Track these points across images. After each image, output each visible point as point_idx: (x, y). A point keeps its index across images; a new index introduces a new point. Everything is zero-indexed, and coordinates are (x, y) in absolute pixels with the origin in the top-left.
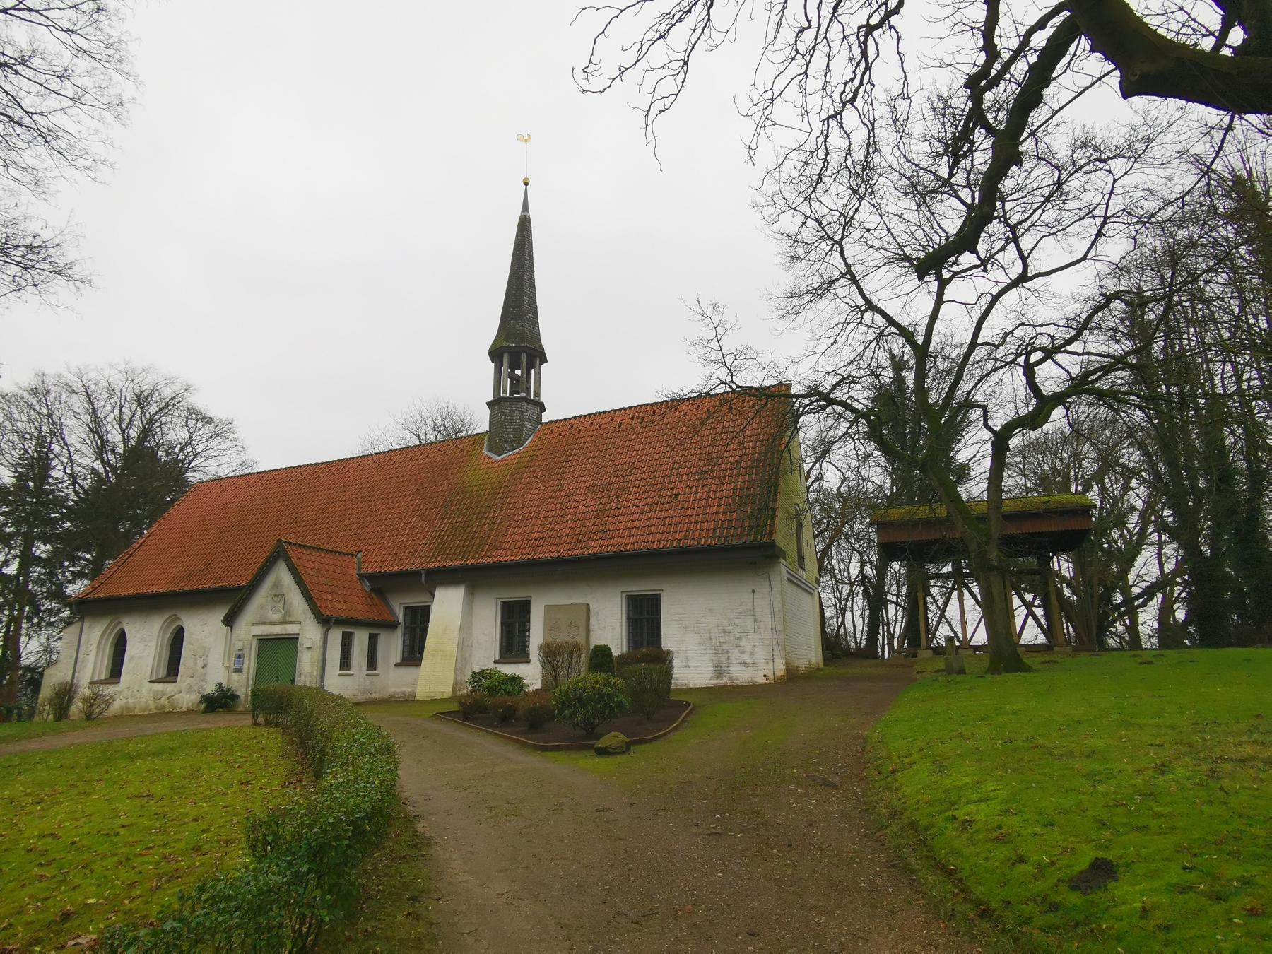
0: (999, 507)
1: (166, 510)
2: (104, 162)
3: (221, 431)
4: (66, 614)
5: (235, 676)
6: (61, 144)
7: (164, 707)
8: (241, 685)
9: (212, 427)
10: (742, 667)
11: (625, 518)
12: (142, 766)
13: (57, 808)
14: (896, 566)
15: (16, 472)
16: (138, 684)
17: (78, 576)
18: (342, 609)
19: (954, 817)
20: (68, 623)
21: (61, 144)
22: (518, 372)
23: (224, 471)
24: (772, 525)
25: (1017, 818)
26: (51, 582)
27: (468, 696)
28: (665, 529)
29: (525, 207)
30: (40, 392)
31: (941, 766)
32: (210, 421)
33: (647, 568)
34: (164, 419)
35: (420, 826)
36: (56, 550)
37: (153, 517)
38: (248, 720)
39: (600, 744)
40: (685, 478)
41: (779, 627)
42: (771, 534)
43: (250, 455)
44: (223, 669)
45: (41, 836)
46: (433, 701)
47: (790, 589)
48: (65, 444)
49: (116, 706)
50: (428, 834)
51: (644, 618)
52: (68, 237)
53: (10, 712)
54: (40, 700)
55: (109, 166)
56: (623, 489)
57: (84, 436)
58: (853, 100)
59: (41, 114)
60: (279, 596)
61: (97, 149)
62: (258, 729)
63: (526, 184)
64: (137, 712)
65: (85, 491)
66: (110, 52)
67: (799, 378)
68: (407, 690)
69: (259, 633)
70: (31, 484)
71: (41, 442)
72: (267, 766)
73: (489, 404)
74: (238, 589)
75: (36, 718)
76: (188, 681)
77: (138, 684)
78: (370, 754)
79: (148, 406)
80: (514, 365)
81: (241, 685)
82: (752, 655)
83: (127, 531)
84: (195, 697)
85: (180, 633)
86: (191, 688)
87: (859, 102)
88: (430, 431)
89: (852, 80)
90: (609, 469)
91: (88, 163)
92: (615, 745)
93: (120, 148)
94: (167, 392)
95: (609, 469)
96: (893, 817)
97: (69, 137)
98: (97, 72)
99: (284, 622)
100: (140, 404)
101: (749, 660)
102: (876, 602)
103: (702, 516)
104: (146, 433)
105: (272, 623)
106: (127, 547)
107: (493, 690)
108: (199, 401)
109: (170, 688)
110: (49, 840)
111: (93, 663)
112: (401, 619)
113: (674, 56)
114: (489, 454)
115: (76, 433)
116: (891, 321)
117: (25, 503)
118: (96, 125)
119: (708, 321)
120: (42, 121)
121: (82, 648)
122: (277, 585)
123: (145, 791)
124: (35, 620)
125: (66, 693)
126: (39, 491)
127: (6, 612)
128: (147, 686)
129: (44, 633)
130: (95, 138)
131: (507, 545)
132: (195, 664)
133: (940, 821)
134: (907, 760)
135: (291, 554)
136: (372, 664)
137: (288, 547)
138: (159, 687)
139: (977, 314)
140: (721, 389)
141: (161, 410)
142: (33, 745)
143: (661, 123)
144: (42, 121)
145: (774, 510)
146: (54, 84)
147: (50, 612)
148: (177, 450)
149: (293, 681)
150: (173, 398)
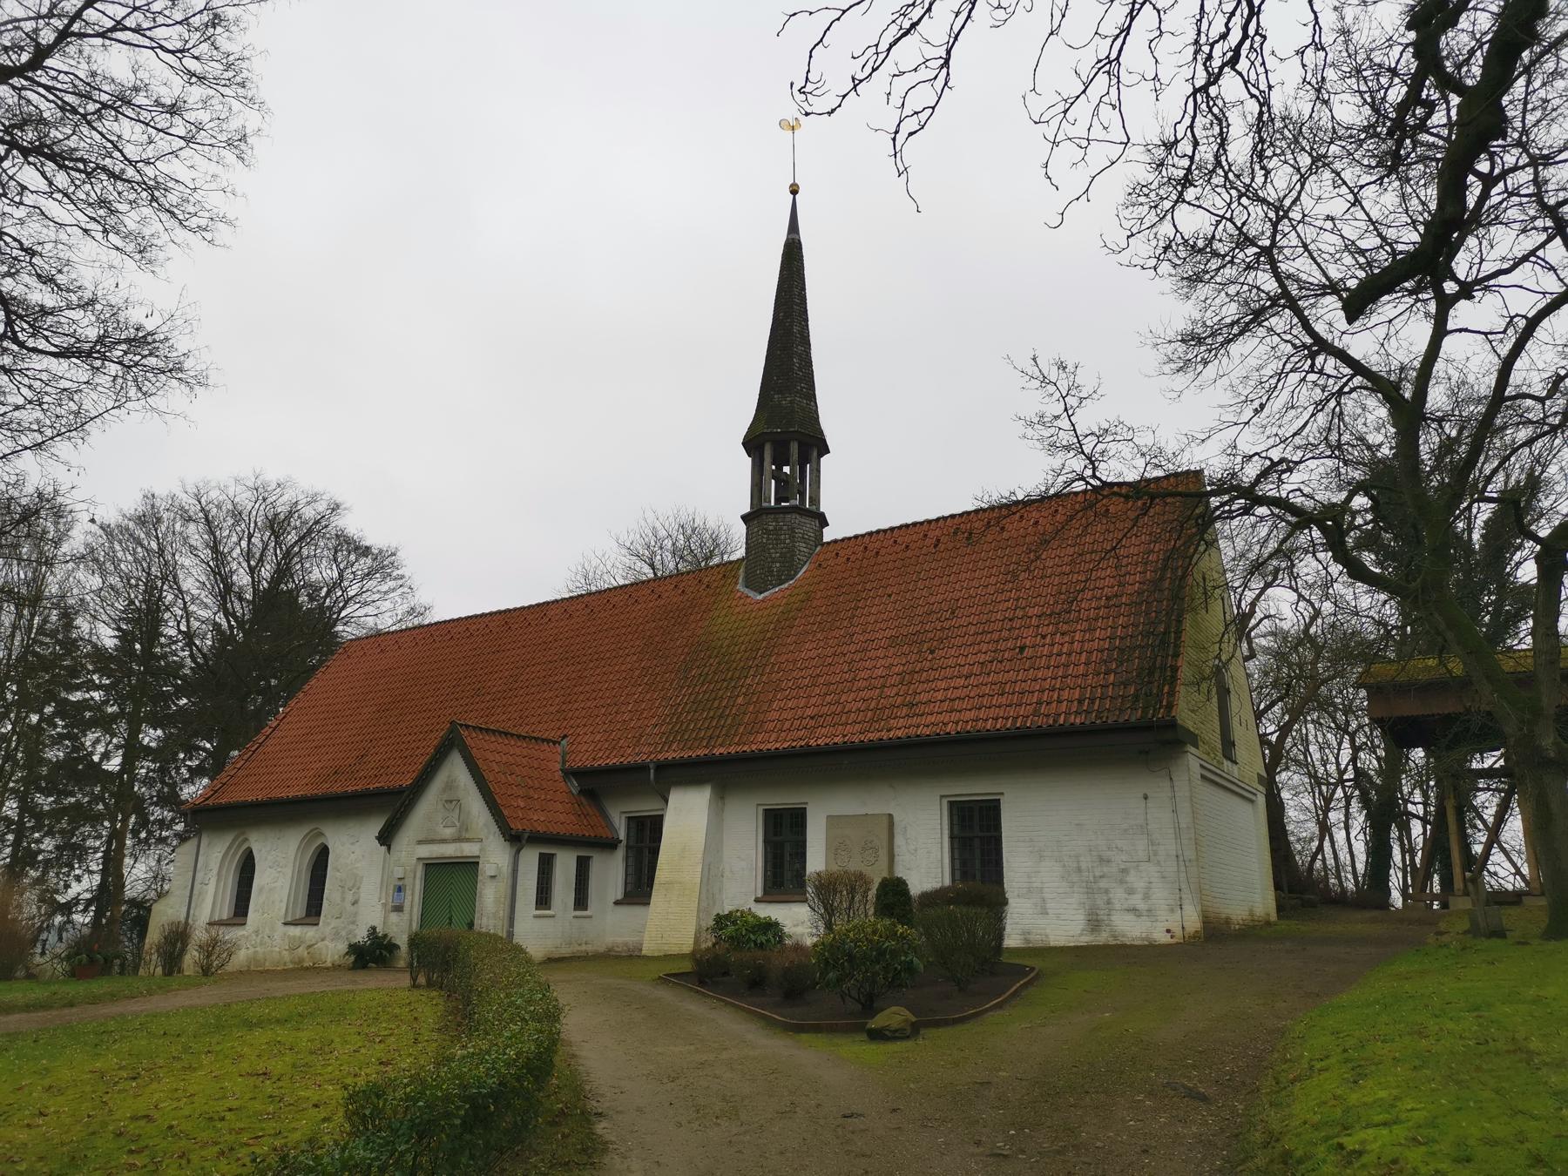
0: (1553, 662)
1: (307, 680)
2: (223, 219)
3: (382, 564)
4: (180, 827)
5: (394, 917)
6: (173, 198)
7: (301, 960)
8: (400, 928)
9: (369, 561)
10: (1130, 917)
11: (943, 685)
12: (260, 1037)
13: (154, 1086)
14: (1418, 754)
15: (119, 629)
16: (269, 931)
17: (196, 773)
18: (539, 821)
19: (1341, 1146)
20: (183, 838)
21: (173, 198)
22: (786, 469)
23: (387, 623)
24: (1172, 693)
25: (1423, 1149)
26: (163, 782)
27: (708, 949)
28: (1003, 700)
29: (793, 226)
30: (149, 519)
31: (1358, 1075)
32: (366, 551)
33: (980, 758)
34: (305, 552)
35: (600, 1128)
36: (168, 737)
37: (290, 690)
38: (406, 980)
39: (875, 1023)
40: (1034, 621)
41: (1190, 854)
42: (1170, 706)
43: (421, 598)
44: (379, 907)
45: (134, 1118)
46: (668, 957)
47: (1206, 791)
48: (179, 589)
49: (241, 957)
50: (608, 1137)
51: (976, 835)
52: (179, 322)
53: (108, 962)
54: (147, 947)
55: (230, 223)
56: (941, 640)
57: (203, 578)
58: (1233, 61)
59: (147, 162)
60: (452, 802)
61: (215, 201)
62: (416, 992)
63: (794, 192)
64: (268, 966)
65: (204, 656)
66: (231, 74)
67: (1211, 460)
68: (631, 939)
69: (426, 855)
70: (138, 646)
71: (150, 588)
72: (416, 1041)
73: (745, 518)
74: (399, 792)
75: (141, 972)
76: (334, 923)
77: (269, 931)
78: (523, 1020)
79: (287, 532)
80: (780, 461)
81: (400, 928)
82: (1146, 897)
83: (258, 710)
84: (342, 947)
85: (322, 856)
86: (337, 933)
87: (1243, 65)
88: (668, 556)
89: (1224, 37)
90: (920, 611)
91: (203, 222)
92: (895, 1026)
93: (244, 195)
94: (309, 513)
95: (920, 611)
96: (1266, 1145)
97: (182, 188)
98: (213, 101)
100: (273, 532)
101: (1142, 906)
102: (1385, 815)
103: (1059, 680)
104: (282, 572)
105: (443, 841)
106: (258, 730)
107: (736, 941)
108: (352, 524)
109: (310, 933)
110: (142, 1123)
111: (213, 899)
112: (622, 835)
113: (931, 52)
114: (746, 591)
115: (193, 576)
116: (1357, 367)
117: (131, 672)
118: (213, 168)
119: (1051, 388)
120: (149, 171)
121: (199, 875)
122: (450, 786)
123: (260, 1068)
124: (143, 835)
125: (178, 937)
126: (148, 654)
127: (106, 824)
128: (281, 929)
129: (155, 852)
130: (213, 186)
131: (771, 726)
132: (343, 899)
133: (1321, 1151)
134: (1318, 1065)
135: (468, 741)
136: (581, 901)
137: (464, 733)
138: (296, 931)
139: (1504, 350)
140: (1079, 486)
141: (301, 539)
142: (134, 1006)
143: (913, 150)
144: (149, 171)
145: (1175, 669)
146: (162, 120)
147: (162, 823)
148: (323, 593)
149: (471, 925)
150: (317, 522)
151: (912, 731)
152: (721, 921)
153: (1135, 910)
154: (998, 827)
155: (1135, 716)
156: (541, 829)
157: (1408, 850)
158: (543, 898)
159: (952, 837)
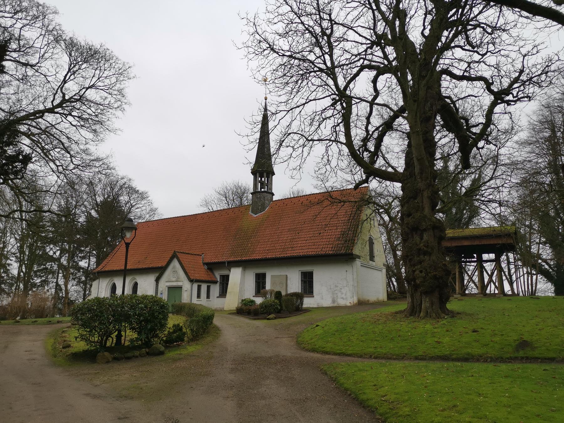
3: (143, 196)
11: (300, 242)
18: (197, 276)
28: (314, 247)
41: (356, 285)
42: (352, 250)
51: (308, 281)
60: (175, 272)
68: (221, 306)
82: (346, 295)
95: (296, 222)
99: (177, 281)
101: (344, 297)
107: (245, 304)
108: (134, 184)
112: (219, 280)
122: (174, 267)
135: (179, 256)
136: (208, 297)
151: (292, 255)
152: (243, 300)
153: (343, 298)
154: (312, 279)
155: (343, 252)
156: (198, 278)
157: (505, 275)
158: (199, 296)
159: (302, 281)
